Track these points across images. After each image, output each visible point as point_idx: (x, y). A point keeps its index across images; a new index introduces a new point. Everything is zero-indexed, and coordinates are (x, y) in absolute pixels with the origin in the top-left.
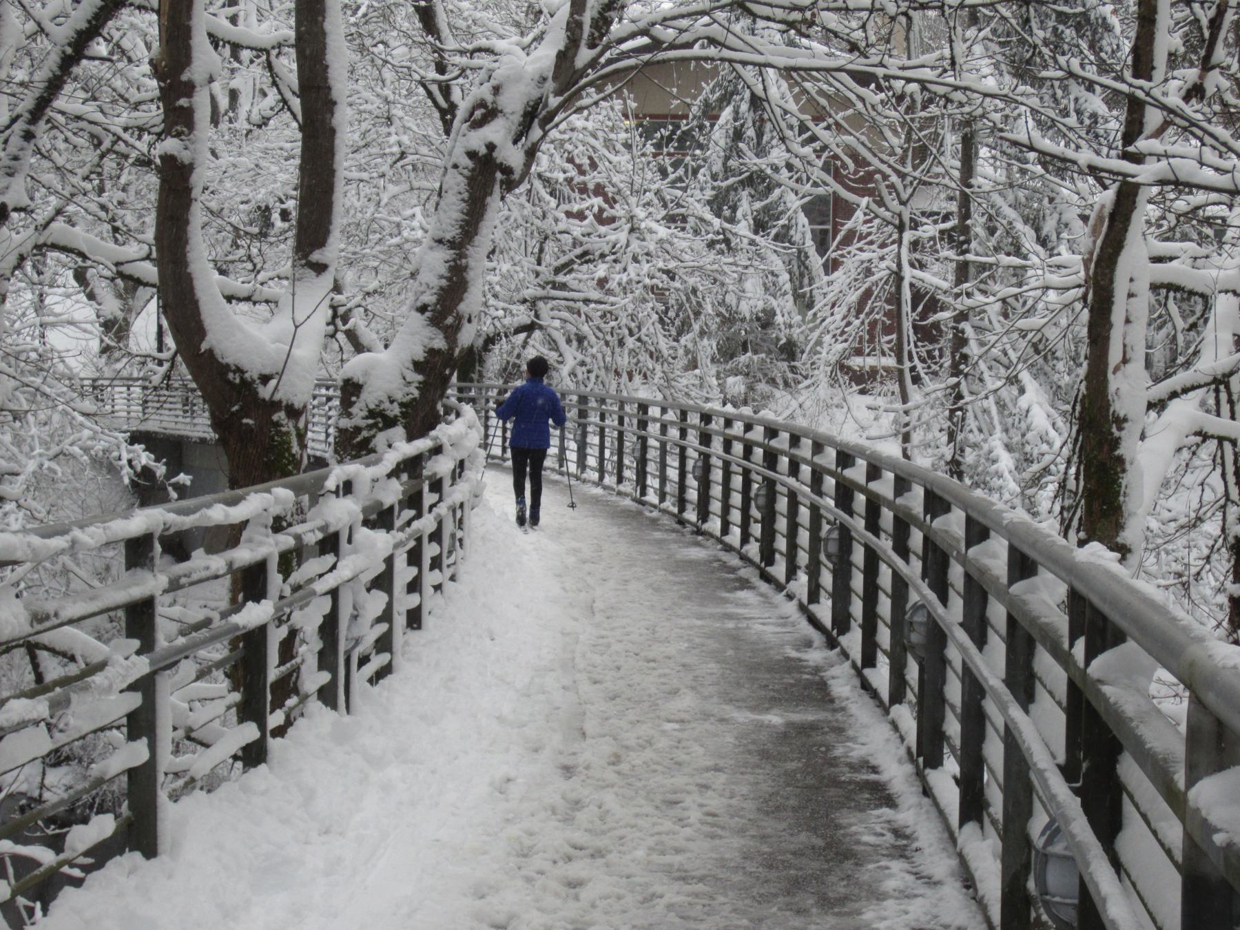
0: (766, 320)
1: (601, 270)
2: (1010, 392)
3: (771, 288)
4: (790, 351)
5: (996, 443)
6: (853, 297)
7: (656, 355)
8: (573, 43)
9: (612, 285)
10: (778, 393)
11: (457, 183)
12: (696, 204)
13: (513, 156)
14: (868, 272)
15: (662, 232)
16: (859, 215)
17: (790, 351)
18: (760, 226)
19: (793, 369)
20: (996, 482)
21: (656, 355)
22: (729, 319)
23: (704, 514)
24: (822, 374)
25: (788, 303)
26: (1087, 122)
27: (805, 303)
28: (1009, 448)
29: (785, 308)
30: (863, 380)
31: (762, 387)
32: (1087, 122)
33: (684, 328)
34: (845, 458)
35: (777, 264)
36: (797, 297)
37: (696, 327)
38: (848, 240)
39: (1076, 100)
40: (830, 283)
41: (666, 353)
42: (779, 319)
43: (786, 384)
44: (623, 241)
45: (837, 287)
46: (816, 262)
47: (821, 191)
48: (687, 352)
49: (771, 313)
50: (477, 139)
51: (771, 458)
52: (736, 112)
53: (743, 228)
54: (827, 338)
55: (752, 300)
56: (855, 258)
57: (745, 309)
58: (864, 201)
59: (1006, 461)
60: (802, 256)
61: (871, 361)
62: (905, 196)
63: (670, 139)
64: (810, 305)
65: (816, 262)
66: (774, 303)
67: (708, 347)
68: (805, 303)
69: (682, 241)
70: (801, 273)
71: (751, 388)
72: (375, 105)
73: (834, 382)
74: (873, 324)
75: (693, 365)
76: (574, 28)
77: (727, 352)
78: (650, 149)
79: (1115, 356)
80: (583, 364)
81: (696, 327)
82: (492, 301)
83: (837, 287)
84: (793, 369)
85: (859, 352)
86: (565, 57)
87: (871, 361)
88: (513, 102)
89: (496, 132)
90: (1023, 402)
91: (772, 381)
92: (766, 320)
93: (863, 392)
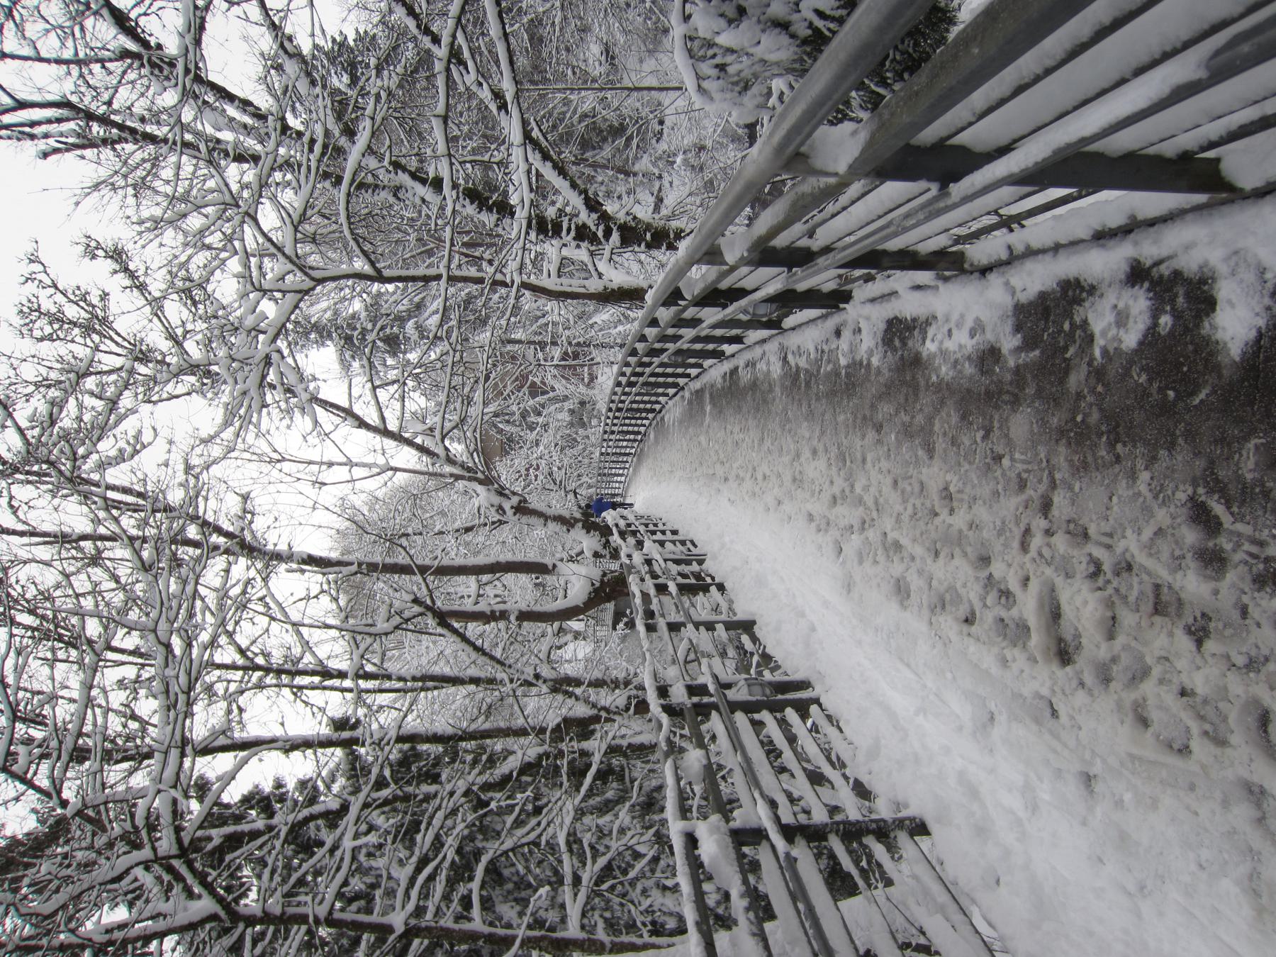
0: (572, 412)
1: (555, 469)
3: (561, 409)
4: (582, 403)
5: (614, 332)
6: (564, 381)
8: (476, 479)
11: (525, 519)
12: (532, 436)
13: (515, 500)
15: (541, 448)
17: (582, 403)
18: (539, 414)
21: (584, 449)
22: (571, 424)
23: (639, 433)
24: (591, 392)
25: (566, 404)
27: (566, 398)
33: (575, 439)
34: (619, 384)
35: (552, 408)
38: (544, 384)
45: (560, 387)
46: (551, 394)
50: (510, 512)
51: (619, 410)
53: (540, 420)
55: (565, 416)
56: (549, 380)
57: (568, 419)
60: (550, 399)
65: (551, 394)
67: (581, 431)
68: (566, 398)
69: (545, 441)
73: (593, 388)
75: (588, 437)
76: (470, 479)
77: (583, 425)
79: (582, 290)
83: (560, 387)
86: (481, 482)
88: (496, 500)
89: (507, 506)
92: (572, 412)
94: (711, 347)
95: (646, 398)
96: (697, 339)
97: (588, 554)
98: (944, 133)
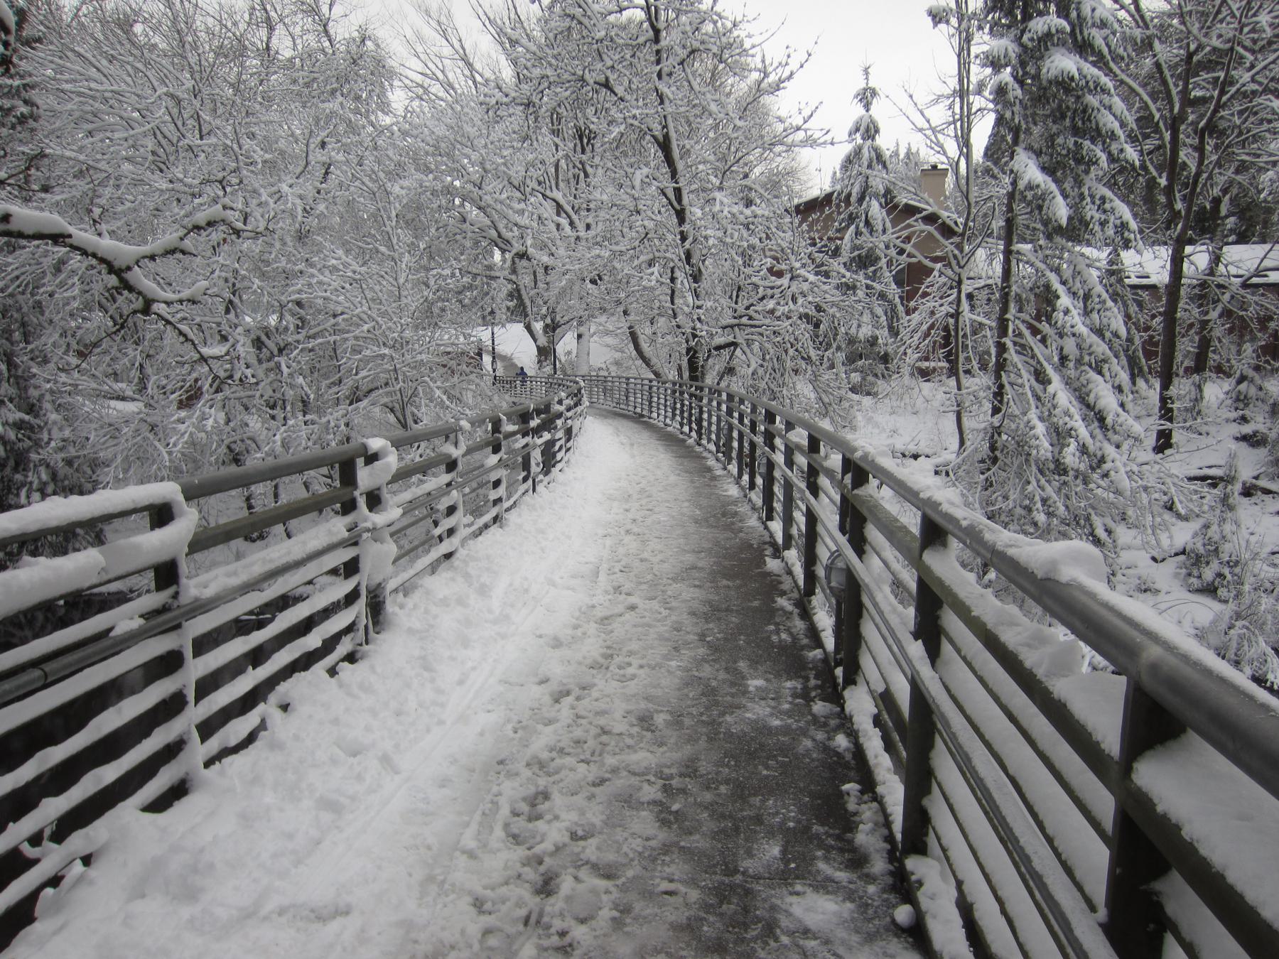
0: (873, 341)
2: (583, 353)
3: (877, 326)
4: (885, 359)
5: (1033, 415)
7: (808, 359)
9: (778, 314)
10: (879, 382)
14: (933, 313)
16: (936, 273)
19: (887, 369)
20: (1033, 442)
21: (808, 359)
22: (852, 341)
24: (906, 370)
25: (886, 332)
26: (1098, 202)
27: (894, 332)
28: (1041, 419)
29: (883, 334)
30: (925, 374)
31: (870, 378)
32: (1098, 202)
33: (829, 346)
35: (879, 311)
36: (891, 328)
37: (834, 346)
38: (925, 295)
39: (1089, 189)
40: (909, 321)
41: (814, 358)
42: (880, 341)
43: (883, 376)
44: (786, 285)
46: (900, 308)
47: (913, 260)
48: (829, 359)
49: (875, 338)
52: (857, 227)
54: (909, 351)
55: (865, 332)
57: (861, 336)
58: (939, 266)
59: (1040, 429)
60: (894, 310)
61: (933, 364)
62: (962, 263)
63: (818, 220)
64: (897, 334)
65: (900, 308)
66: (878, 332)
67: (840, 357)
68: (894, 332)
70: (892, 315)
71: (864, 379)
72: (630, 204)
73: (912, 375)
74: (935, 342)
75: (832, 367)
77: (851, 359)
78: (805, 227)
80: (762, 366)
81: (834, 346)
82: (699, 325)
84: (887, 369)
85: (927, 359)
87: (933, 364)
90: (1051, 389)
91: (876, 375)
92: (873, 341)
93: (928, 381)
94: (778, 506)
95: (714, 428)
96: (788, 486)
97: (292, 327)
98: (953, 634)
